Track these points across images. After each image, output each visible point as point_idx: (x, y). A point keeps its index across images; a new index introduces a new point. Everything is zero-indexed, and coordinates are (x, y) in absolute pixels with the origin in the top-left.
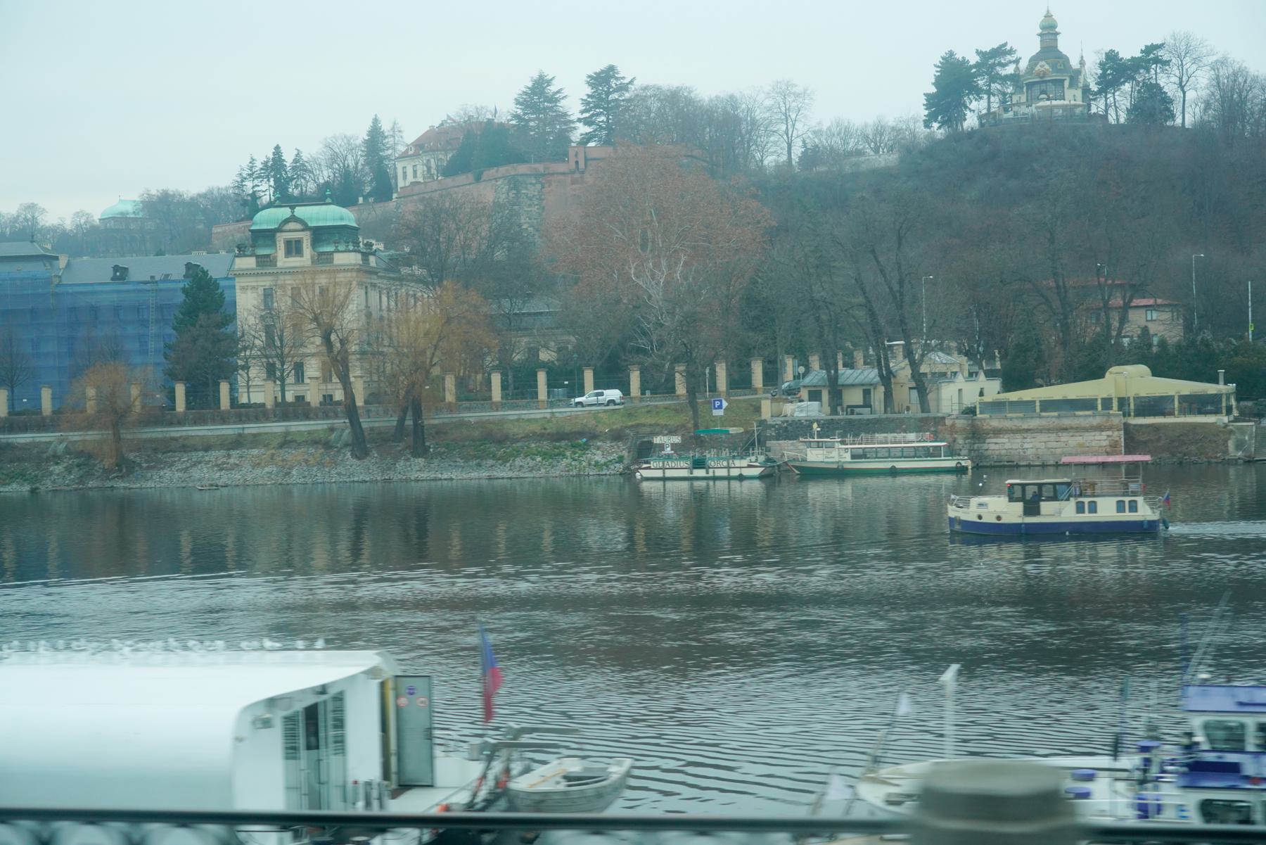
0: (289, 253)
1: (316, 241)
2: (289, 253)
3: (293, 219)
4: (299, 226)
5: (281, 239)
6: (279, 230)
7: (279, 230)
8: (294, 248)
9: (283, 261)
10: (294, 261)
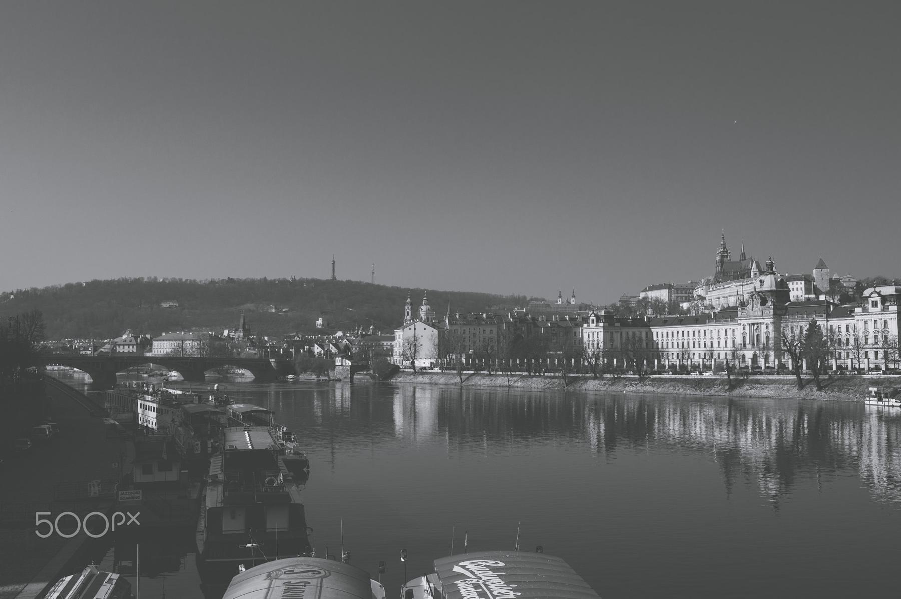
0: (873, 306)
1: (883, 303)
2: (873, 306)
5: (871, 300)
6: (870, 296)
7: (870, 296)
8: (875, 304)
9: (871, 309)
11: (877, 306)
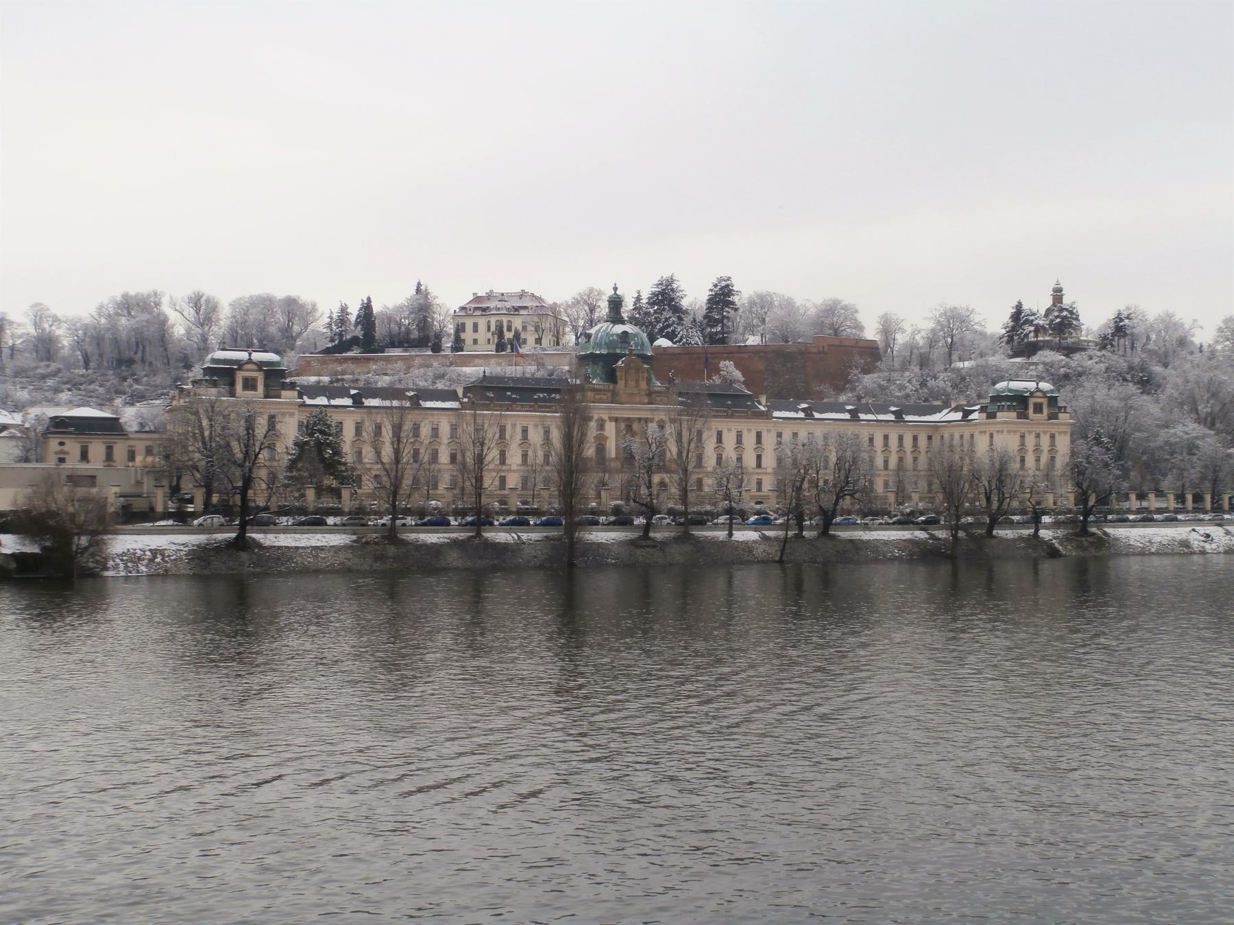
0: (1035, 412)
1: (1049, 405)
2: (1035, 412)
3: (1038, 390)
4: (254, 367)
10: (1038, 416)
11: (254, 388)
